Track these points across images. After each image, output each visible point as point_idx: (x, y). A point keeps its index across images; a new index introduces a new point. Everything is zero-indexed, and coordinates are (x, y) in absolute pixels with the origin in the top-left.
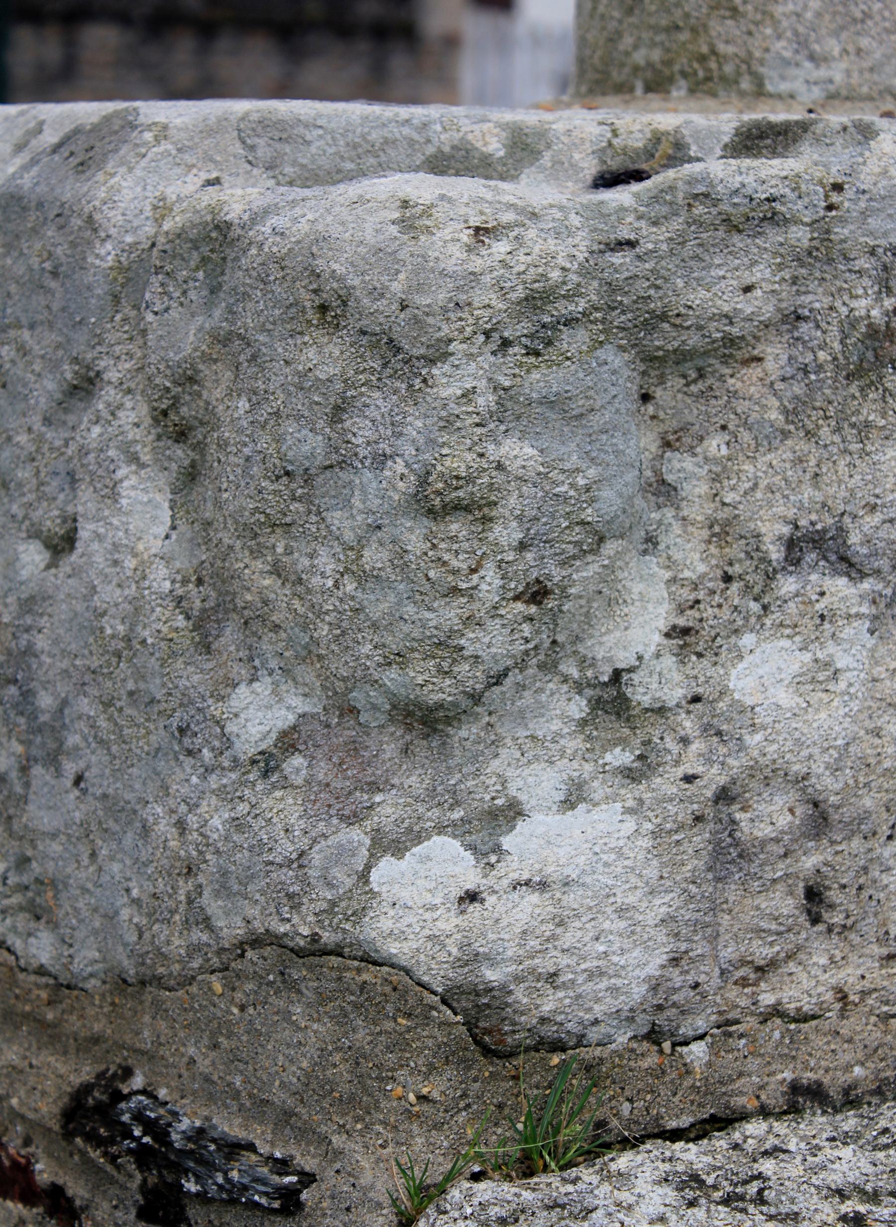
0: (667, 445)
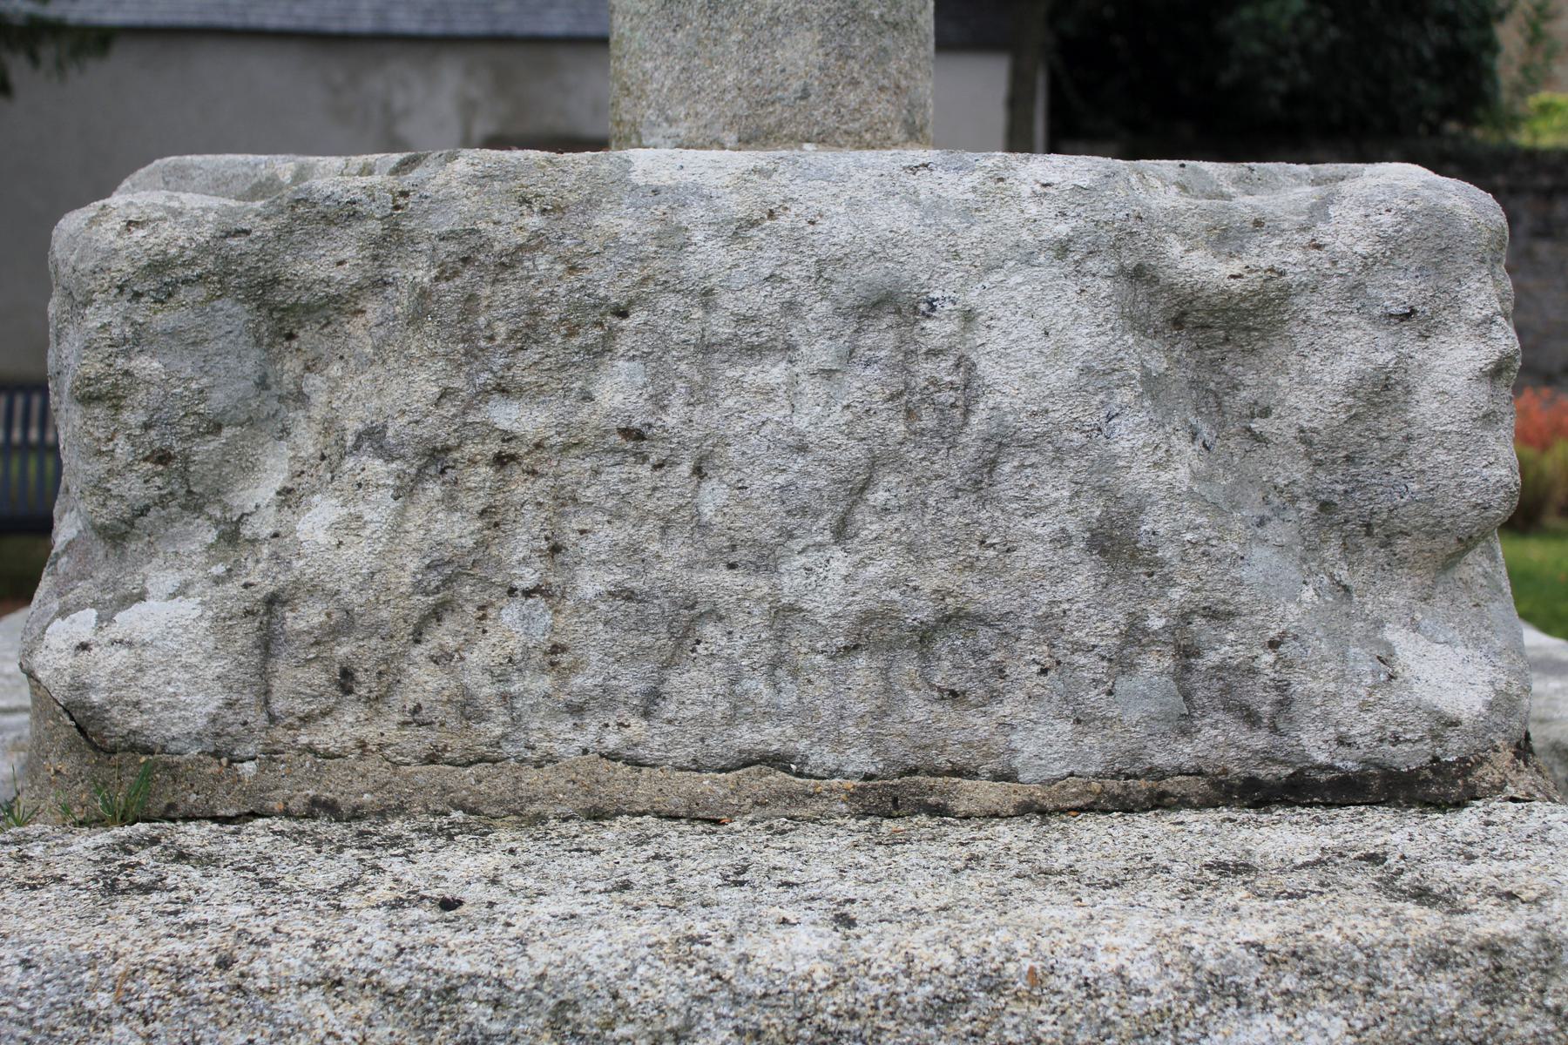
0: (308, 368)
